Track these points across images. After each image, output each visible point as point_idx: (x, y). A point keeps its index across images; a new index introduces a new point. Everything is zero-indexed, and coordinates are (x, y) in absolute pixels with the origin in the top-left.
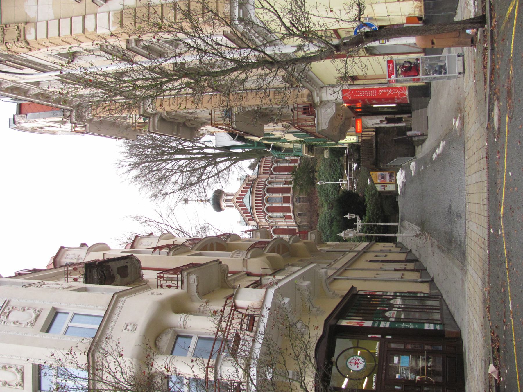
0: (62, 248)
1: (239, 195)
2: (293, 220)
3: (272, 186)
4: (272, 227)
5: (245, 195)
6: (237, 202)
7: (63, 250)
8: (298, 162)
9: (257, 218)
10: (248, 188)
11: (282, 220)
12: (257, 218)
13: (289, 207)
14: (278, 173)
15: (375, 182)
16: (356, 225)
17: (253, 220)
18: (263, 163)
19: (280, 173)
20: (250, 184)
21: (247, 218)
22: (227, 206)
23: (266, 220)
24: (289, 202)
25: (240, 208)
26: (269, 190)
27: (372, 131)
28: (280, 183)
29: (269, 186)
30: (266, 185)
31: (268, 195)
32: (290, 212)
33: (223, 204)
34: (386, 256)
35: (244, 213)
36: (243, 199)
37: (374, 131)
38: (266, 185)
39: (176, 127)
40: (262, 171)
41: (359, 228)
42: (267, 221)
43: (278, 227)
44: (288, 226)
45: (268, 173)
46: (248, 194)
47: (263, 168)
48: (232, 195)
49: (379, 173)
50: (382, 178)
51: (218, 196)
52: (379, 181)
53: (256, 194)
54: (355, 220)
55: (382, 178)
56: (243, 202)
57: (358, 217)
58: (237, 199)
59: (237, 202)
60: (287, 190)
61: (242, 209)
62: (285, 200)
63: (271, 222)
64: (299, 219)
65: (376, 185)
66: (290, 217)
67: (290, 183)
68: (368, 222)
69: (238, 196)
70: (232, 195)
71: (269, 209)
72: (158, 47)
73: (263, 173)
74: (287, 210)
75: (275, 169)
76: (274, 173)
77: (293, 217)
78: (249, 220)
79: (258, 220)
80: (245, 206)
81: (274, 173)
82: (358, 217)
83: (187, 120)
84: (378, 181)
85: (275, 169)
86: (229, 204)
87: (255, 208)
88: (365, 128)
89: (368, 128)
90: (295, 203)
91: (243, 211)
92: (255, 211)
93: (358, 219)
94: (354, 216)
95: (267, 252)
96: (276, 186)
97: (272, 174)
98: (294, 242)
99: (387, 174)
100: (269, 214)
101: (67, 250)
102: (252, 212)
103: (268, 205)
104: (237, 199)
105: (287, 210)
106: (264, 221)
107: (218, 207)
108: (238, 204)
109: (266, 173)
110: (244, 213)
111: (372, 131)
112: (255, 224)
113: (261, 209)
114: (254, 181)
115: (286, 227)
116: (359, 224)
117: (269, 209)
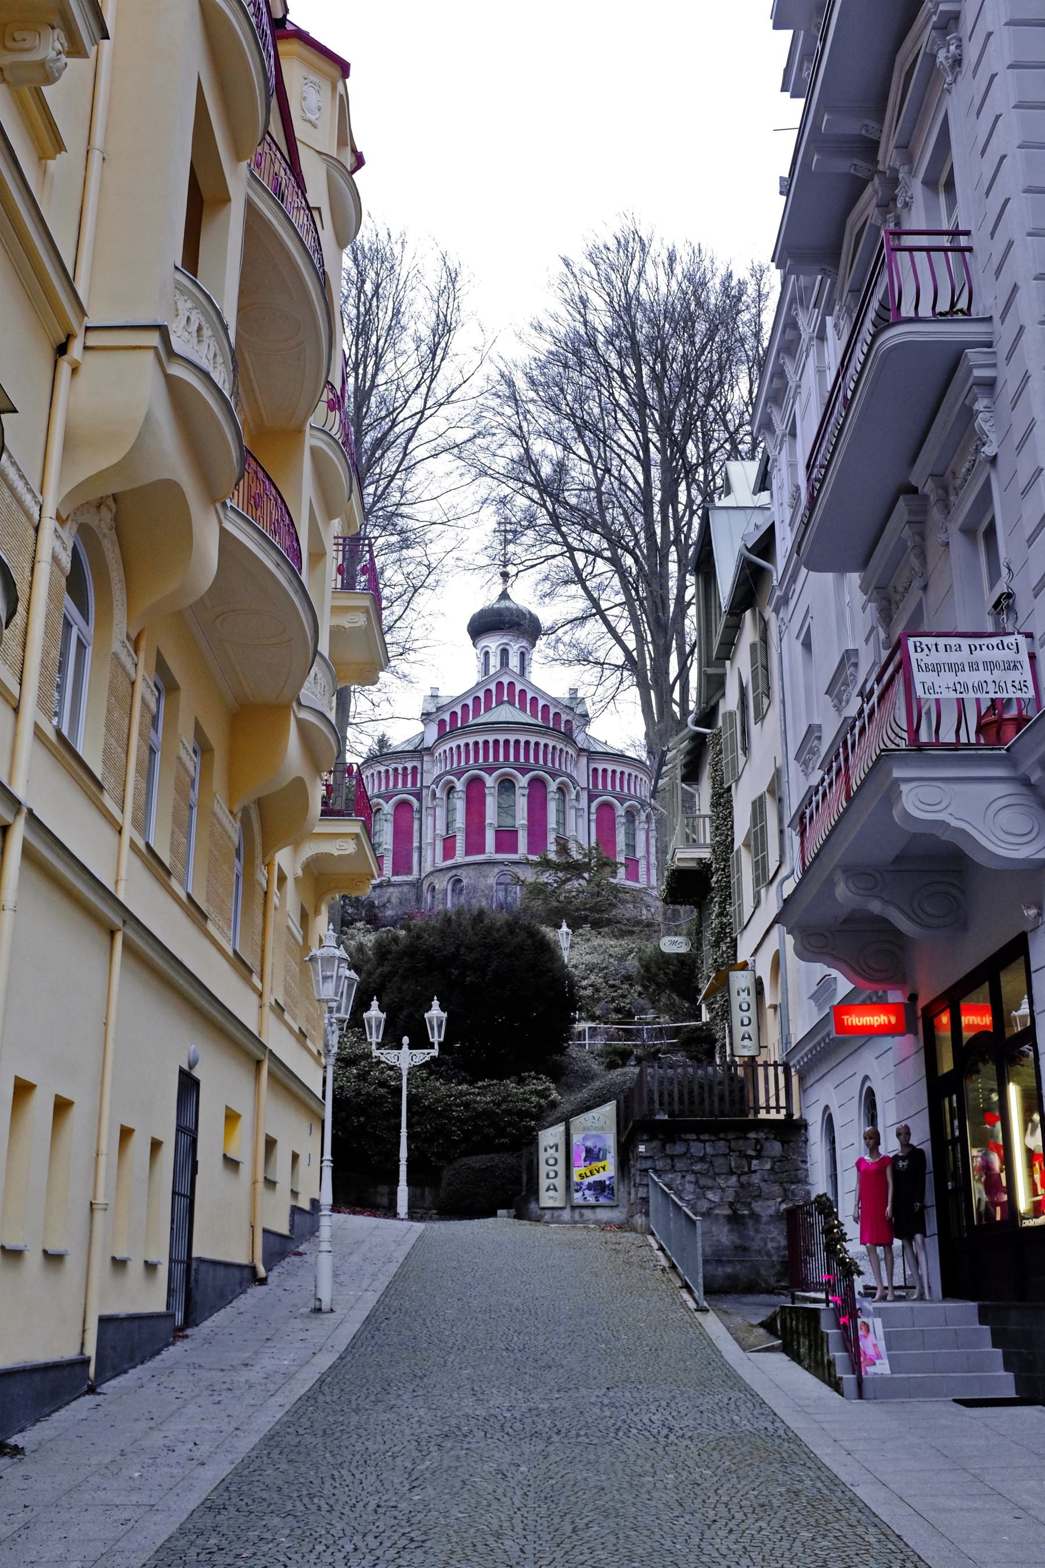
0: (344, 68)
1: (523, 692)
2: (441, 864)
3: (550, 796)
4: (418, 796)
5: (523, 709)
6: (500, 685)
7: (336, 72)
8: (629, 883)
9: (447, 747)
10: (545, 718)
11: (441, 830)
12: (447, 747)
13: (481, 850)
14: (593, 817)
15: (577, 1122)
16: (399, 1047)
17: (442, 735)
18: (627, 771)
19: (593, 825)
20: (563, 722)
21: (447, 717)
22: (487, 653)
23: (440, 777)
24: (499, 849)
25: (481, 694)
26: (537, 785)
27: (789, 1107)
28: (562, 823)
29: (553, 786)
30: (554, 776)
31: (523, 781)
32: (468, 852)
33: (493, 643)
34: (231, 1164)
35: (465, 707)
36: (511, 703)
37: (789, 1115)
38: (554, 776)
39: (852, 126)
40: (600, 767)
41: (389, 1056)
42: (437, 781)
43: (416, 816)
44: (420, 848)
45: (595, 785)
46: (526, 718)
47: (610, 768)
48: (523, 668)
49: (610, 1141)
50: (588, 1151)
51: (521, 626)
52: (576, 1139)
53: (527, 743)
54: (420, 1041)
55: (588, 1151)
56: (500, 703)
57: (435, 1052)
58: (511, 684)
59: (500, 685)
60: (537, 839)
61: (477, 699)
62: (506, 840)
63: (434, 794)
64: (442, 883)
65: (561, 1128)
66: (449, 851)
67: (563, 848)
68: (412, 1100)
69: (518, 687)
70: (523, 668)
71: (475, 786)
72: (967, 465)
73: (595, 770)
74: (475, 845)
75: (606, 806)
76: (594, 805)
77: (449, 863)
78: (442, 723)
79: (441, 750)
80: (488, 708)
81: (594, 805)
82: (435, 1052)
83: (894, 182)
84: (578, 1144)
85: (606, 806)
86: (495, 662)
87: (481, 739)
88: (802, 1079)
89: (803, 1090)
90: (496, 870)
91: (470, 702)
92: (471, 740)
93: (421, 1056)
94: (436, 1038)
95: (225, 536)
96: (552, 807)
97: (591, 798)
98: (301, 724)
99: (608, 1170)
100: (460, 785)
101: (334, 88)
102: (466, 729)
103: (490, 781)
104: (511, 684)
105: (475, 845)
106: (437, 771)
107: (481, 626)
108: (493, 687)
109: (595, 778)
110: (465, 707)
111: (789, 1107)
112: (429, 742)
113: (476, 759)
114: (568, 737)
115: (416, 844)
116: (405, 1058)
117: (475, 786)
